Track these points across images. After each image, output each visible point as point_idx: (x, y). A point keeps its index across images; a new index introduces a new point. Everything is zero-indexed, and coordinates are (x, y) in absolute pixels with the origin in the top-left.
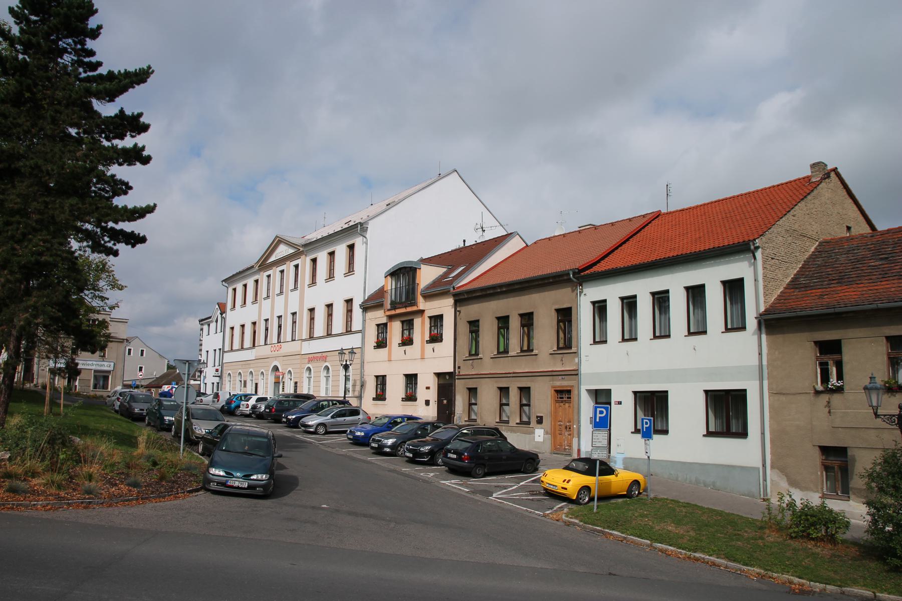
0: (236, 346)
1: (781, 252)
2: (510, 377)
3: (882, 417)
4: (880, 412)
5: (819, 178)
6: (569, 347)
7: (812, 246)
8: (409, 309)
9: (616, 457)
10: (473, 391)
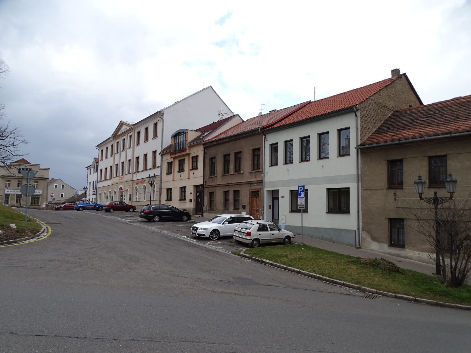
0: (103, 179)
1: (371, 114)
2: (230, 185)
3: (424, 199)
4: (423, 197)
5: (395, 78)
6: (258, 168)
7: (390, 113)
8: (183, 153)
9: (281, 225)
10: (211, 194)
